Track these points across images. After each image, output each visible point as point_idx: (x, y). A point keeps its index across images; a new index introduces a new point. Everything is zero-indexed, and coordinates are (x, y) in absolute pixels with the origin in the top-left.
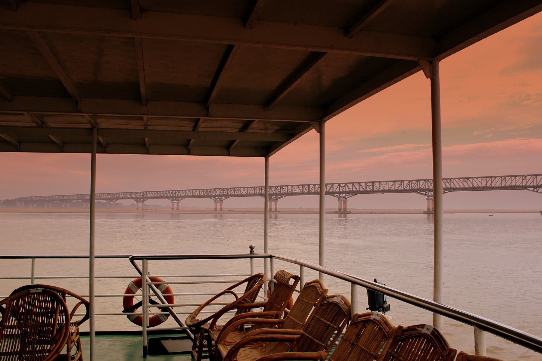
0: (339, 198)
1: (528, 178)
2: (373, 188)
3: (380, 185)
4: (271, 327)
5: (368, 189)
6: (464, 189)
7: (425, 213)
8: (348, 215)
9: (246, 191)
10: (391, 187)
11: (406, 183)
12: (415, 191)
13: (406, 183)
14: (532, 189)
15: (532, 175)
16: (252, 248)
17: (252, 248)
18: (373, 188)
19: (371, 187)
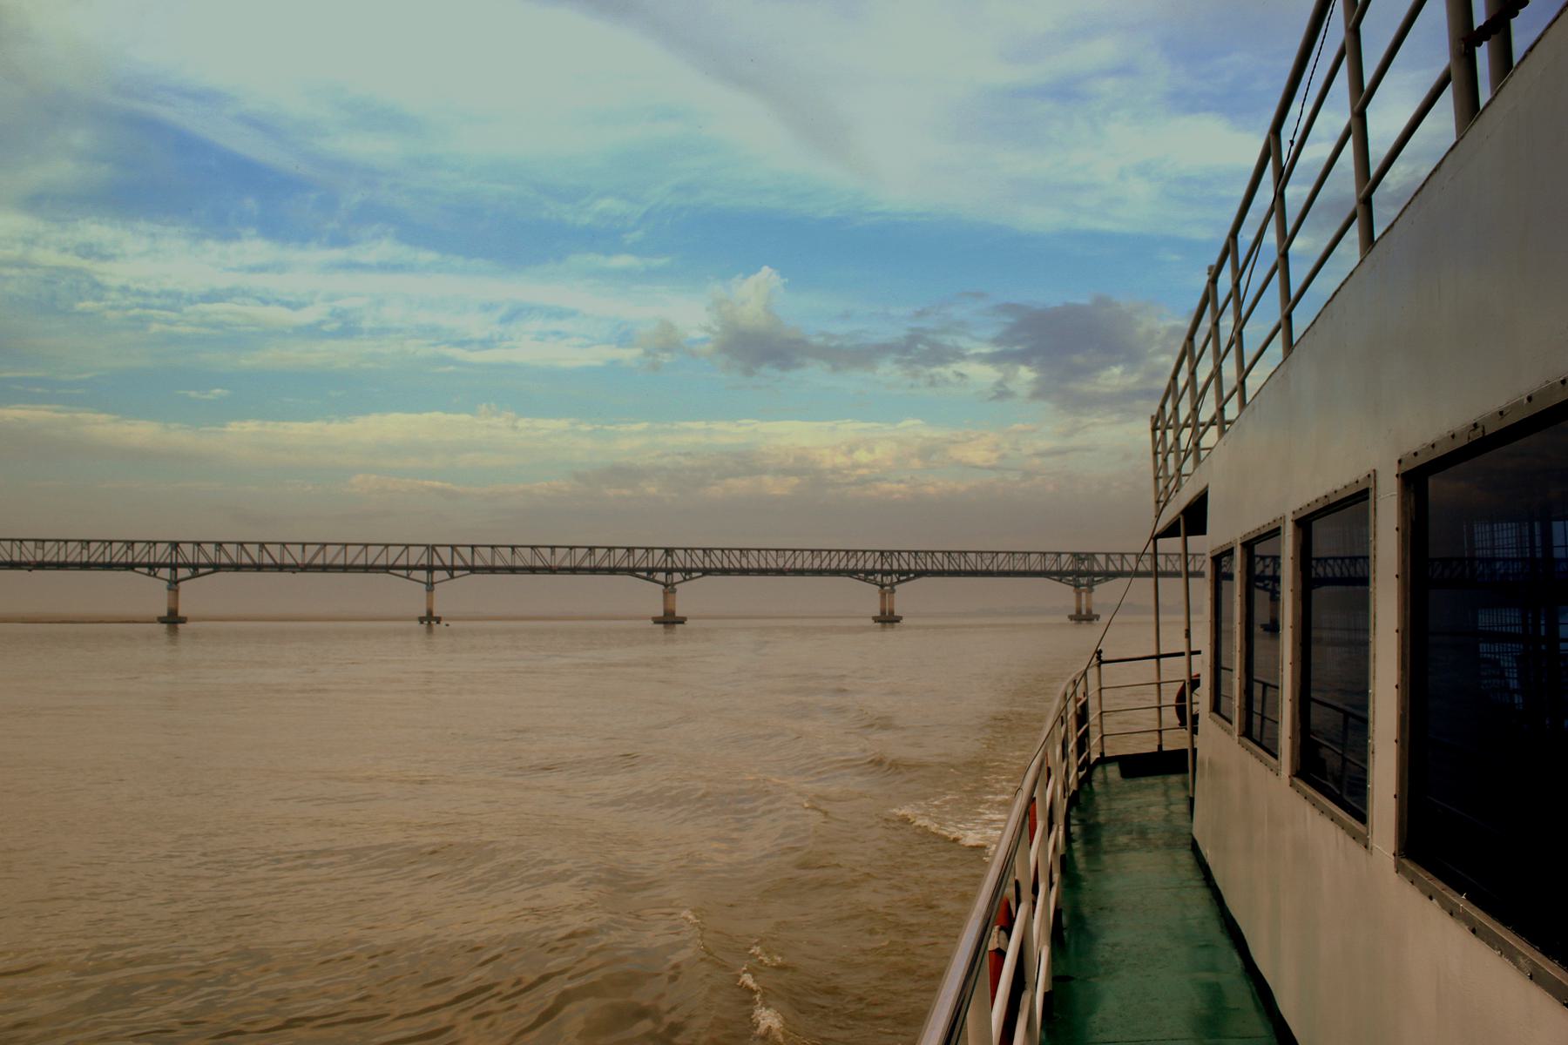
0: (1077, 586)
1: (93, 546)
2: (282, 556)
3: (553, 553)
4: (1272, 687)
5: (1111, 568)
6: (780, 572)
7: (162, 620)
8: (180, 626)
9: (807, 562)
10: (564, 559)
11: (619, 553)
12: (852, 573)
13: (311, 550)
14: (146, 570)
15: (103, 542)
16: (1199, 652)
17: (1199, 652)
18: (282, 556)
19: (1118, 564)
